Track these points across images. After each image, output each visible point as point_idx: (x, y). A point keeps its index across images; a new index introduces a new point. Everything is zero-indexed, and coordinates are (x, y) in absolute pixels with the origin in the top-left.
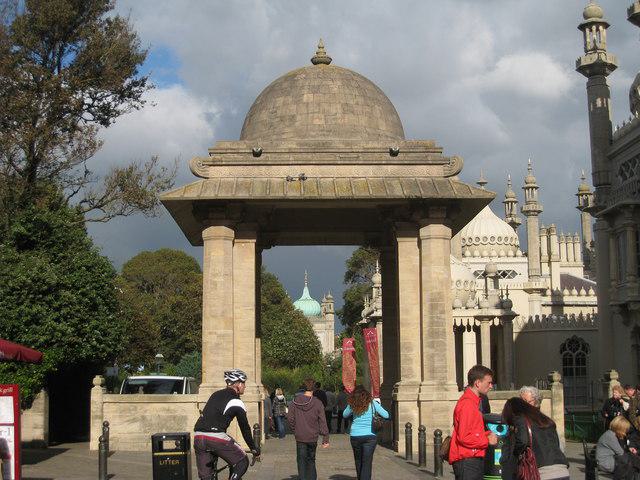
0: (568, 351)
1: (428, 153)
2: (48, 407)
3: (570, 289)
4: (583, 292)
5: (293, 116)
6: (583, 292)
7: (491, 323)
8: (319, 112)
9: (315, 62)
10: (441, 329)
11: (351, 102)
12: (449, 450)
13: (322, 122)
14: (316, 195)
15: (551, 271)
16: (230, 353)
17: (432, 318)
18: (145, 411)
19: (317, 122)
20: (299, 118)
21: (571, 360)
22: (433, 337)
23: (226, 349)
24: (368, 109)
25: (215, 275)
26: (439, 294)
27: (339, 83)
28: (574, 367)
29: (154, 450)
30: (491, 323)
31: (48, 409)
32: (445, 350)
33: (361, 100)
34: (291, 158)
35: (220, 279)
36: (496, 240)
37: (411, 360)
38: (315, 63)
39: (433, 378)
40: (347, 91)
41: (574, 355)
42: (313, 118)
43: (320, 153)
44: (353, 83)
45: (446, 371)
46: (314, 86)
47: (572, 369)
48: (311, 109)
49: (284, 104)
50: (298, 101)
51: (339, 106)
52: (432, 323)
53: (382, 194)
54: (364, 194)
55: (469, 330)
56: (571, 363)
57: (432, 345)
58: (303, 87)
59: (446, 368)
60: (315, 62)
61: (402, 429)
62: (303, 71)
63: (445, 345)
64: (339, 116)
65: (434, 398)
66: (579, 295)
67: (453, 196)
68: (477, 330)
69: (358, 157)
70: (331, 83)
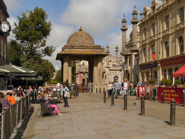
1: (99, 47)
9: (80, 30)
37: (96, 79)
43: (83, 47)
52: (99, 73)
60: (80, 30)
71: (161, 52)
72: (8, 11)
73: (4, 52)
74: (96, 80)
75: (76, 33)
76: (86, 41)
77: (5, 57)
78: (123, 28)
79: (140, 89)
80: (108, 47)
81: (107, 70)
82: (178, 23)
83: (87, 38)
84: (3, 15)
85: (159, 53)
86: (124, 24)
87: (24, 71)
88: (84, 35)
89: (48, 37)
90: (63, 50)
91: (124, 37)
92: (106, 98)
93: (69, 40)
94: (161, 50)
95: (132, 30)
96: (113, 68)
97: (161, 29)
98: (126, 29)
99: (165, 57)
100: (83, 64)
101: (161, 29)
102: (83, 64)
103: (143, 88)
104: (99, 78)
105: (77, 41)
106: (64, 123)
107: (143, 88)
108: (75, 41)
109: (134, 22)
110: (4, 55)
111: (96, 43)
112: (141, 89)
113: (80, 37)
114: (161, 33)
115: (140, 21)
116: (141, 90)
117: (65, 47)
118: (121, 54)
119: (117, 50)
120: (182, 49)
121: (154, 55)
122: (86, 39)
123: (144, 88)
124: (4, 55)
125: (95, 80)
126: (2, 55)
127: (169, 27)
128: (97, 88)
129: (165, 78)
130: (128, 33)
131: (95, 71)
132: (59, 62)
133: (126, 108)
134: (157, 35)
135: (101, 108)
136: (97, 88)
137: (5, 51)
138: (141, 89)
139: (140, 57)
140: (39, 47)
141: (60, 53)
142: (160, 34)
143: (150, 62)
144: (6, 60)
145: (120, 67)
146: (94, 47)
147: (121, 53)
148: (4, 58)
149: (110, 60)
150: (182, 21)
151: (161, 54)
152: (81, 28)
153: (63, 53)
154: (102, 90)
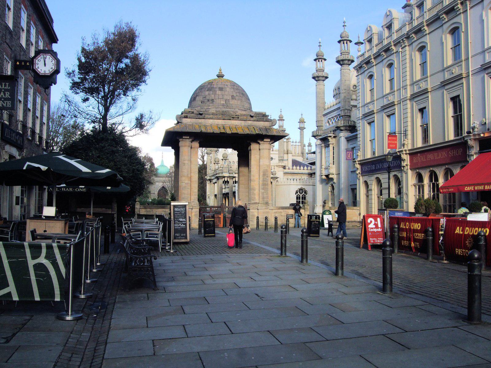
0: (299, 193)
1: (263, 117)
2: (430, 179)
3: (296, 166)
4: (302, 168)
6: (302, 168)
7: (223, 180)
9: (218, 76)
10: (267, 183)
12: (166, 266)
15: (288, 158)
16: (190, 190)
18: (156, 212)
21: (300, 197)
22: (264, 186)
23: (188, 189)
25: (184, 160)
28: (301, 200)
30: (223, 180)
35: (186, 162)
37: (255, 194)
38: (218, 77)
41: (301, 195)
43: (225, 116)
45: (268, 199)
47: (300, 201)
49: (209, 94)
50: (215, 94)
52: (264, 181)
56: (300, 199)
57: (263, 189)
60: (218, 76)
62: (215, 80)
66: (300, 169)
71: (409, 133)
72: (57, 28)
73: (42, 124)
74: (257, 197)
75: (210, 83)
76: (232, 102)
77: (45, 136)
78: (316, 74)
79: (369, 221)
80: (281, 119)
81: (280, 173)
82: (417, 79)
83: (235, 95)
84: (45, 36)
85: (406, 135)
86: (320, 64)
87: (84, 169)
88: (230, 86)
89: (142, 87)
90: (178, 123)
91: (320, 96)
92: (243, 234)
93: (193, 99)
94: (409, 128)
95: (339, 78)
96: (293, 169)
97: (408, 78)
98: (351, 59)
99: (419, 143)
100: (225, 158)
101: (408, 78)
102: (225, 158)
103: (376, 220)
104: (263, 193)
105: (213, 100)
106: (186, 309)
107: (376, 220)
108: (208, 100)
109: (372, 40)
110: (41, 131)
111: (256, 108)
112: (371, 222)
113: (219, 92)
114: (408, 87)
115: (358, 58)
116: (371, 226)
117: (183, 115)
118: (313, 136)
119: (302, 125)
120: (425, 133)
121: (393, 140)
122: (233, 98)
123: (379, 219)
124: (41, 131)
125: (255, 198)
126: (20, 117)
127: (427, 73)
128: (258, 218)
129: (434, 198)
130: (329, 86)
131: (254, 176)
132: (170, 152)
133: (388, 286)
134: (399, 90)
135: (276, 269)
136: (258, 218)
137: (45, 120)
138: (371, 222)
139: (358, 143)
140: (123, 114)
141: (172, 130)
142: (405, 87)
143: (385, 155)
144: (47, 143)
145: (309, 168)
146: (252, 117)
147: (313, 132)
148: (41, 138)
149: (286, 150)
150: (423, 75)
151: (409, 137)
152: (220, 70)
153: (179, 129)
154: (272, 222)
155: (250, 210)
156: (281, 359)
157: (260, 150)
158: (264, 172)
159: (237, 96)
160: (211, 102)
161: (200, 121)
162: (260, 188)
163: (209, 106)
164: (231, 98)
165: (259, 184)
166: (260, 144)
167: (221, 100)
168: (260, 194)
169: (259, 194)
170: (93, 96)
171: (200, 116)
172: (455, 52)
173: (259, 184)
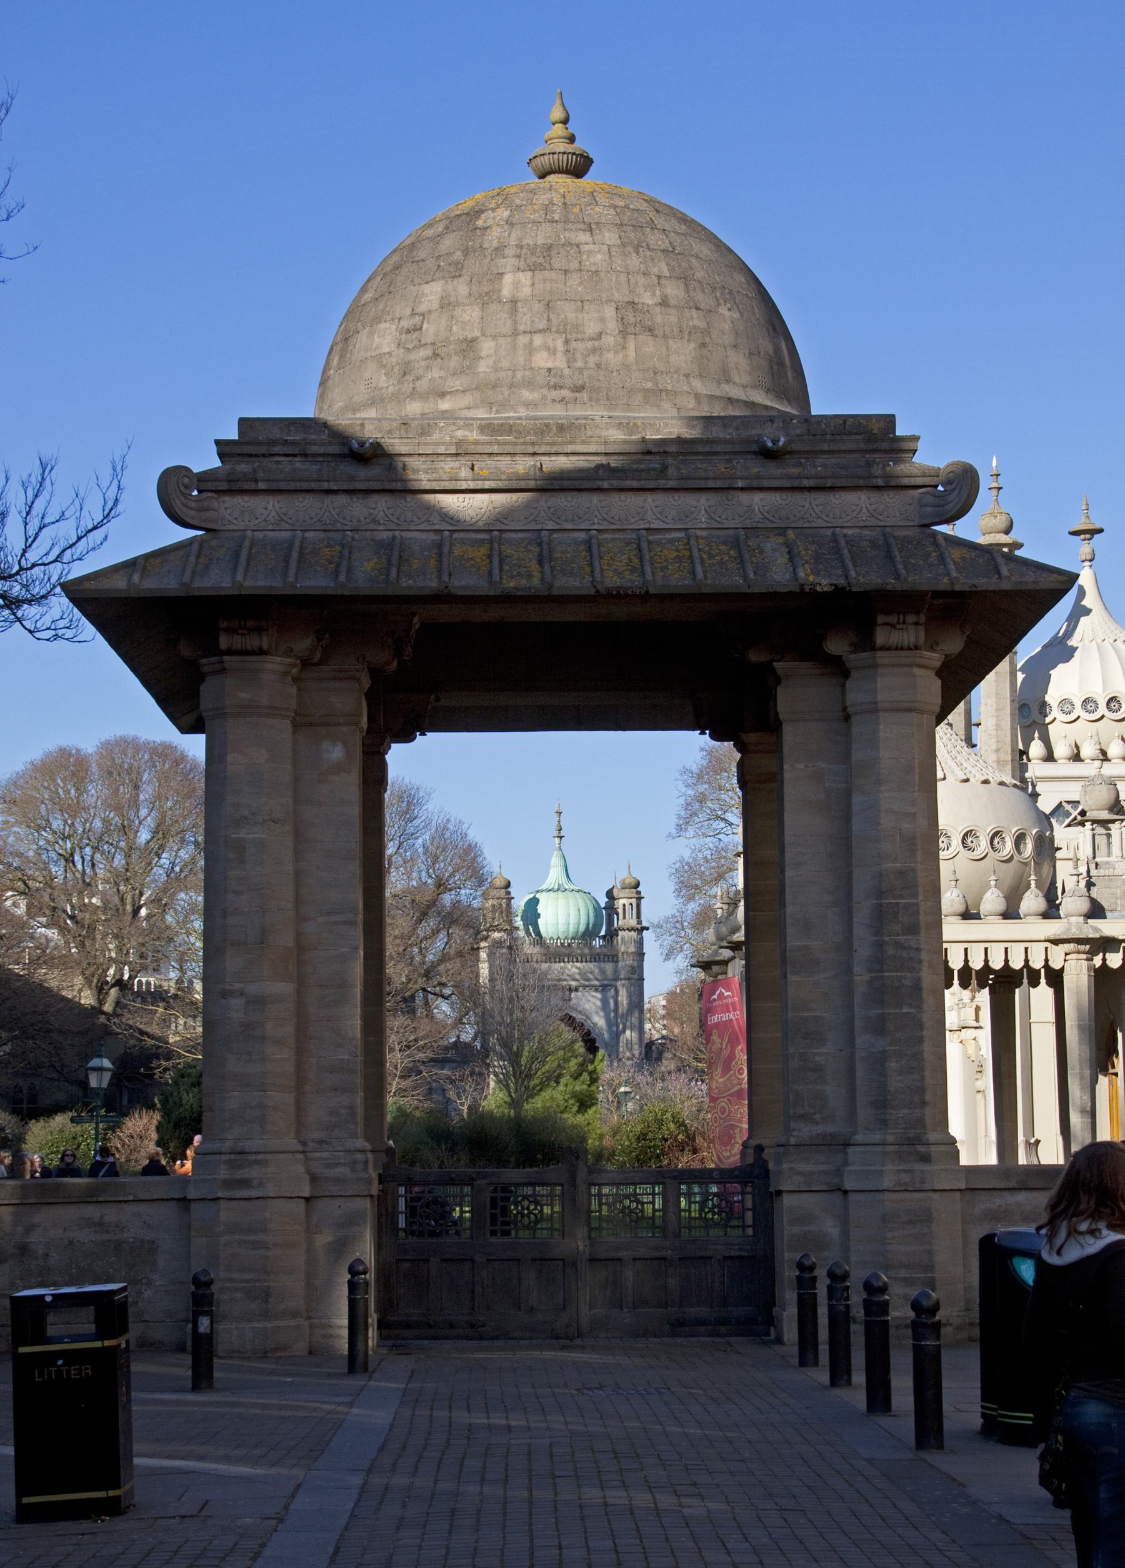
5: (472, 343)
8: (547, 330)
11: (648, 299)
13: (560, 362)
14: (536, 582)
17: (879, 946)
19: (542, 360)
20: (487, 347)
24: (697, 320)
26: (901, 873)
27: (610, 237)
29: (19, 1339)
31: (777, 1265)
32: (921, 1040)
33: (675, 291)
34: (718, 448)
36: (1102, 710)
39: (883, 1123)
40: (634, 261)
42: (530, 350)
44: (655, 239)
46: (533, 250)
48: (525, 320)
49: (446, 304)
51: (610, 312)
52: (878, 962)
53: (732, 580)
54: (677, 579)
55: (1034, 982)
57: (879, 1027)
58: (499, 250)
59: (922, 1091)
61: (788, 1273)
63: (920, 1026)
64: (609, 340)
65: (888, 1182)
67: (944, 584)
68: (1055, 978)
69: (665, 468)
70: (583, 237)
155: (785, 1196)
156: (1057, 1437)
157: (847, 718)
158: (880, 893)
159: (664, 303)
160: (454, 362)
161: (358, 509)
162: (858, 1023)
163: (443, 395)
164: (612, 325)
165: (848, 990)
166: (846, 674)
167: (538, 340)
168: (860, 1072)
169: (851, 1070)
170: (333, 563)
171: (349, 468)
172: (379, 1236)
173: (848, 990)
